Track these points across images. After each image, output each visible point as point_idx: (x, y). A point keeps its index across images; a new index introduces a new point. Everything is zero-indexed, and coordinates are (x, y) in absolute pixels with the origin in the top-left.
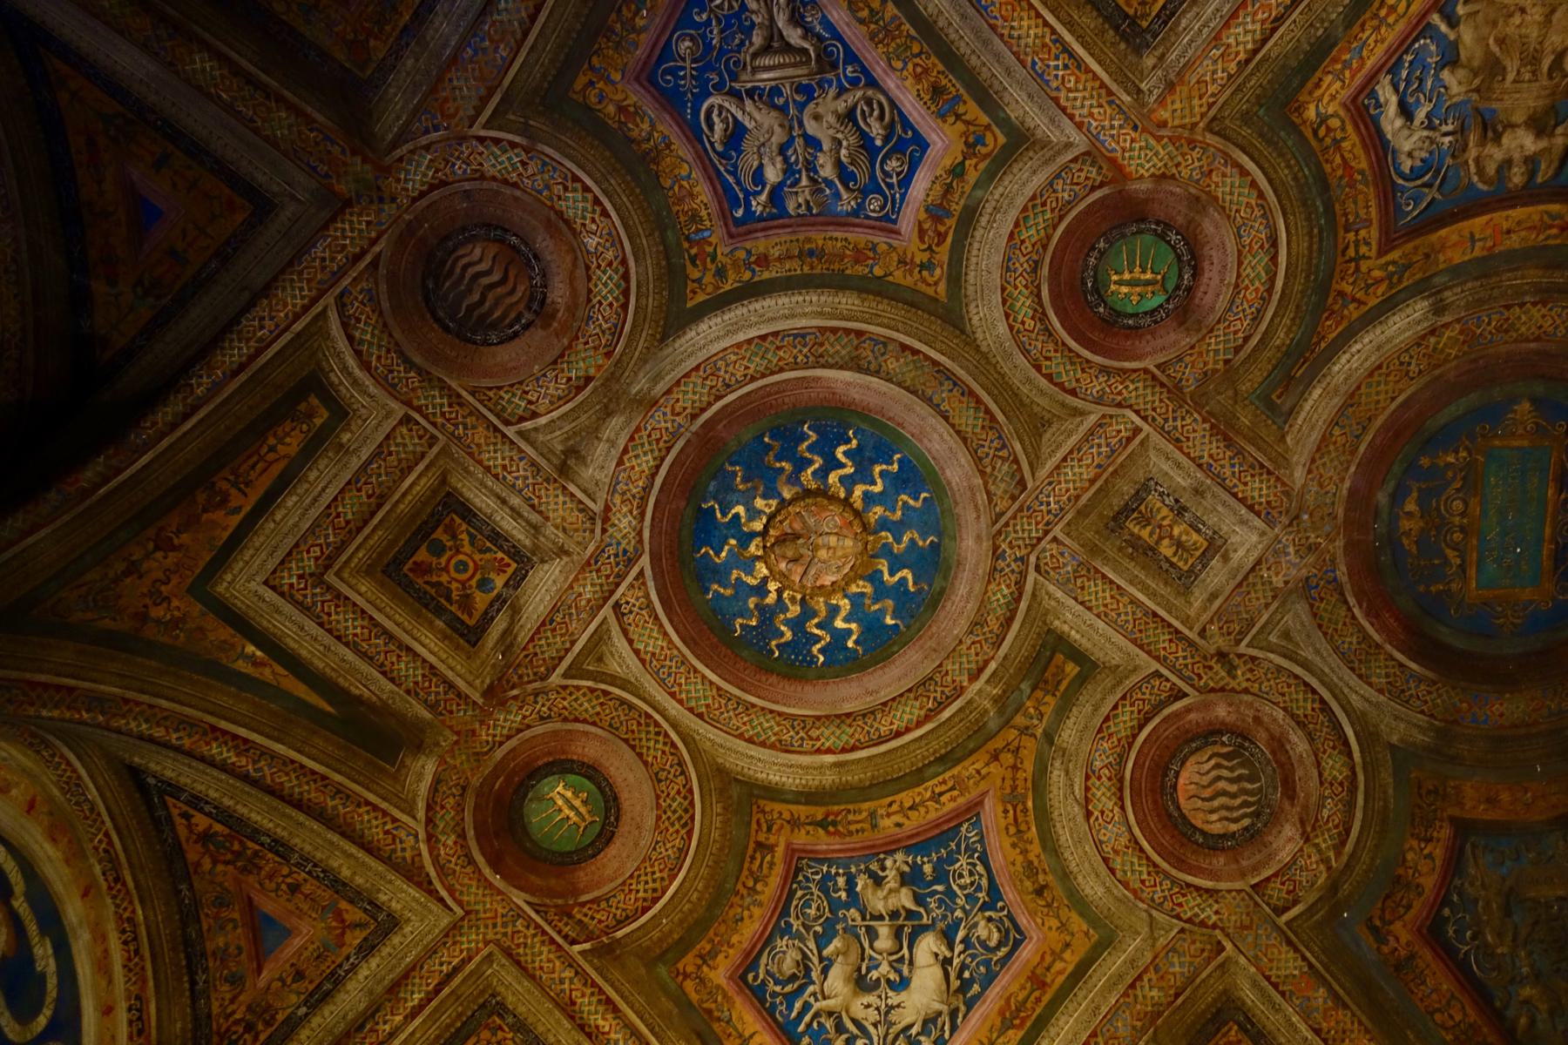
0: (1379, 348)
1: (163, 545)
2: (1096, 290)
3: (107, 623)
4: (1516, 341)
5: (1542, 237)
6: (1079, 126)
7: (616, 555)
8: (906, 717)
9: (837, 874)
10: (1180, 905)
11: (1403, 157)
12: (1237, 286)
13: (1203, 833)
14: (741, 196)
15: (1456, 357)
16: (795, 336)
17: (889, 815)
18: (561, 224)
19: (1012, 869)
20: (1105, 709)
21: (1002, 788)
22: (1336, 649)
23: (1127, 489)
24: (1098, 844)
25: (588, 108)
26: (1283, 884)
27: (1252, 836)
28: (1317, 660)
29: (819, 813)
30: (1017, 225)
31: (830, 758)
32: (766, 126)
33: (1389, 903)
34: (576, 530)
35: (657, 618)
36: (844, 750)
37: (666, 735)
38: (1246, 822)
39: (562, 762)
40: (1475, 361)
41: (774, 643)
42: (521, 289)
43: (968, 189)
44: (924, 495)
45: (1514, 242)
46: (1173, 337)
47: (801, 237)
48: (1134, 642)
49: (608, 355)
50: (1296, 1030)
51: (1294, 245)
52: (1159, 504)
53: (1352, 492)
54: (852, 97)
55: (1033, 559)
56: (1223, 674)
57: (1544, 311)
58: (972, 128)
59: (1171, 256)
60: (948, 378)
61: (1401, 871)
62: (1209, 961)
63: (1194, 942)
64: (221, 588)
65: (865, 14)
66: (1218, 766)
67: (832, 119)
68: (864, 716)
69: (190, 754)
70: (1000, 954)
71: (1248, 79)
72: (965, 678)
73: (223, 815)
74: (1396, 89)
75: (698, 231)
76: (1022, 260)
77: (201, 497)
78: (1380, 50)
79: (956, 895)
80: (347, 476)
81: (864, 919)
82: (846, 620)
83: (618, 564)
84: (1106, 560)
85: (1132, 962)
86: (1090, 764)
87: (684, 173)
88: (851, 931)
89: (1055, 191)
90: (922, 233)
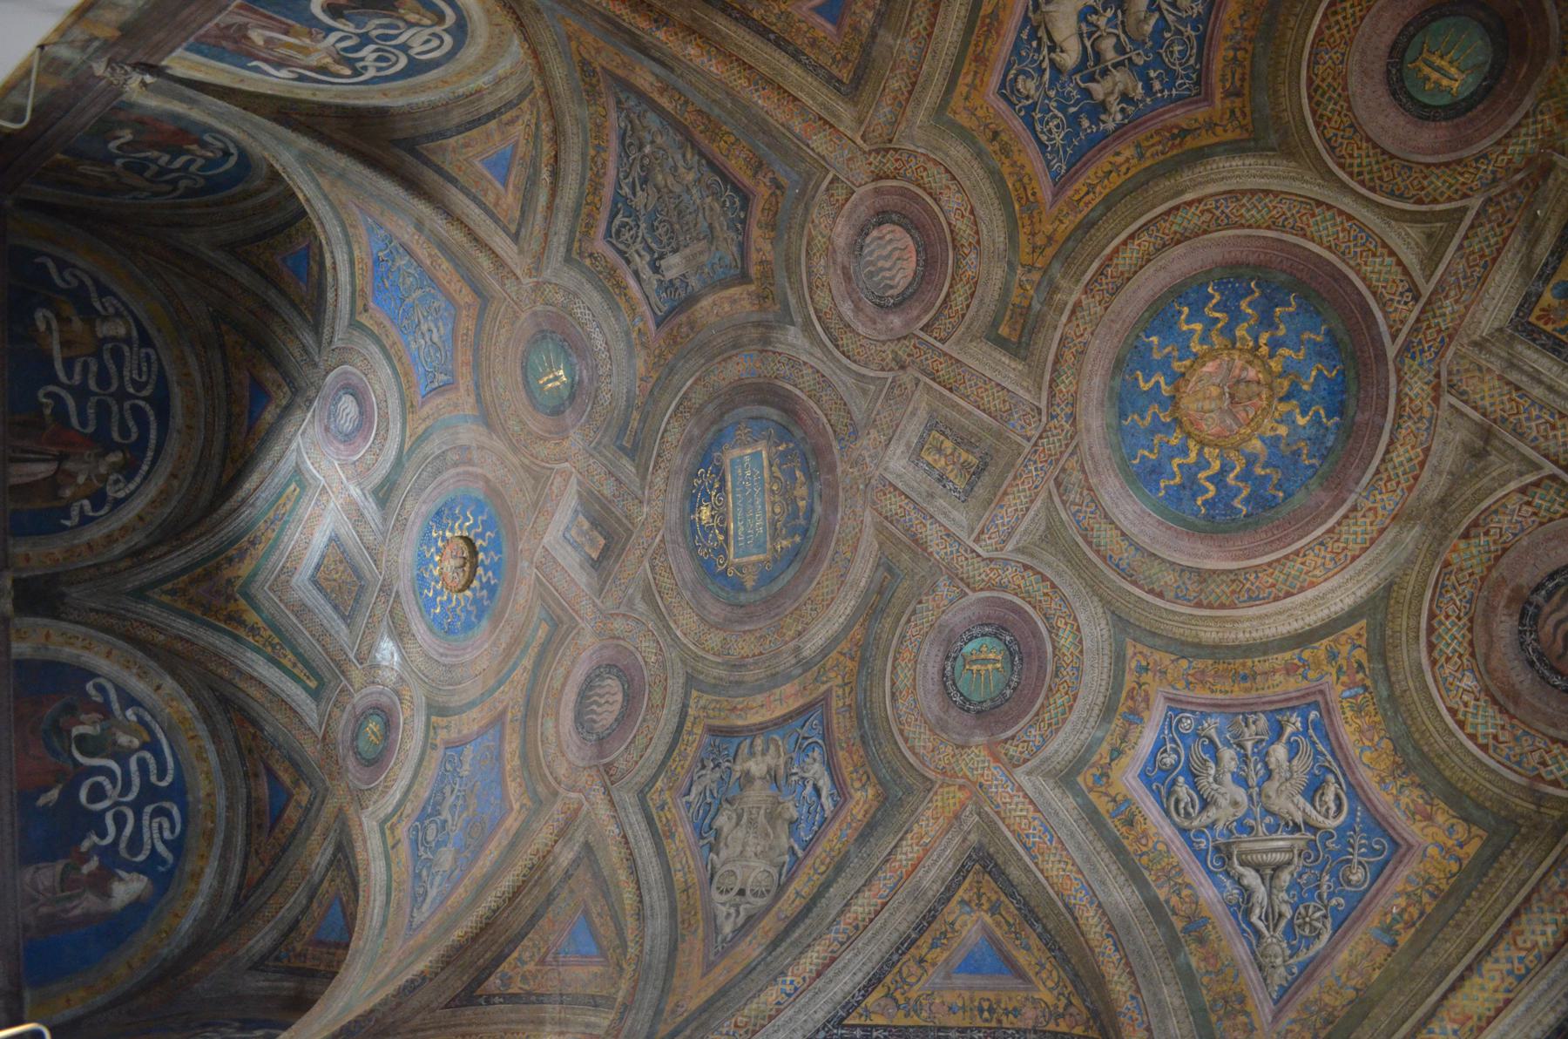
6: (1020, 788)
7: (1422, 351)
8: (1128, 254)
9: (1162, 91)
10: (897, 160)
12: (916, 662)
13: (893, 223)
14: (1311, 731)
16: (1257, 598)
17: (1127, 160)
18: (1501, 699)
19: (1020, 147)
20: (975, 302)
21: (1040, 213)
23: (981, 491)
24: (961, 189)
25: (1467, 819)
28: (845, 378)
29: (1190, 143)
30: (1071, 707)
31: (1188, 197)
32: (1283, 797)
34: (1467, 370)
35: (1374, 294)
36: (1177, 208)
37: (1351, 175)
38: (868, 240)
39: (1458, 115)
41: (1257, 294)
42: (1549, 627)
43: (1108, 738)
44: (1136, 462)
45: (760, 699)
47: (1254, 694)
49: (1447, 564)
52: (956, 481)
53: (836, 510)
54: (1204, 819)
55: (1044, 419)
56: (900, 353)
58: (1103, 789)
60: (1123, 570)
61: (772, 234)
65: (1185, 892)
66: (892, 278)
67: (1223, 802)
68: (1164, 245)
70: (1013, 72)
71: (907, 819)
72: (1084, 303)
75: (1355, 697)
76: (1067, 678)
78: (830, 835)
79: (1057, 108)
81: (1130, 59)
83: (1420, 343)
84: (989, 430)
85: (918, 103)
86: (979, 254)
87: (1368, 753)
88: (1138, 43)
90: (1147, 700)
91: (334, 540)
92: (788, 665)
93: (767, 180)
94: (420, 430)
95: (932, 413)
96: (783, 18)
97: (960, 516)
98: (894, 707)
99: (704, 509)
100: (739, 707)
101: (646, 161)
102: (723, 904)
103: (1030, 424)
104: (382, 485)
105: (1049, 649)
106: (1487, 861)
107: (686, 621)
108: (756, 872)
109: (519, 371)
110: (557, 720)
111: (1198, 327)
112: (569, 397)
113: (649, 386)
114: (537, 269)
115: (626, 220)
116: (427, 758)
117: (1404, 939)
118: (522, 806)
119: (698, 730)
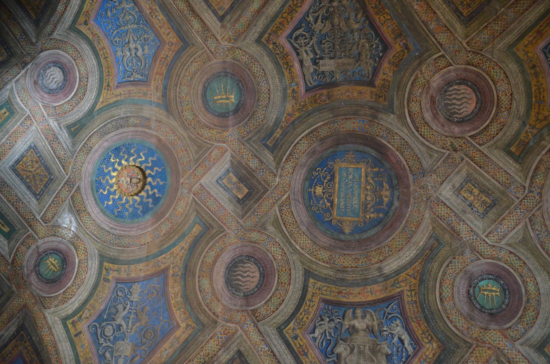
0: (399, 257)
2: (504, 290)
5: (348, 290)
6: (519, 352)
10: (480, 60)
11: (400, 325)
13: (467, 85)
15: (372, 251)
21: (544, 106)
22: (413, 150)
23: (491, 215)
24: (509, 83)
26: (439, 66)
27: (449, 83)
28: (419, 146)
30: (537, 318)
33: (401, 58)
38: (451, 89)
45: (357, 290)
46: (475, 269)
48: (488, 158)
50: (441, 13)
51: (434, 298)
52: (479, 208)
53: (408, 206)
55: (526, 192)
56: (455, 143)
57: (344, 264)
59: (478, 299)
61: (395, 69)
62: (472, 39)
63: (478, 46)
66: (459, 110)
74: (406, 349)
76: (533, 304)
84: (498, 189)
85: (502, 39)
86: (509, 114)
89: (524, 328)
91: (33, 148)
93: (401, 44)
94: (112, 101)
99: (318, 188)
100: (344, 292)
103: (519, 192)
104: (74, 124)
109: (200, 88)
110: (211, 280)
112: (234, 110)
113: (293, 119)
114: (235, 40)
116: (100, 285)
118: (187, 326)
119: (316, 300)
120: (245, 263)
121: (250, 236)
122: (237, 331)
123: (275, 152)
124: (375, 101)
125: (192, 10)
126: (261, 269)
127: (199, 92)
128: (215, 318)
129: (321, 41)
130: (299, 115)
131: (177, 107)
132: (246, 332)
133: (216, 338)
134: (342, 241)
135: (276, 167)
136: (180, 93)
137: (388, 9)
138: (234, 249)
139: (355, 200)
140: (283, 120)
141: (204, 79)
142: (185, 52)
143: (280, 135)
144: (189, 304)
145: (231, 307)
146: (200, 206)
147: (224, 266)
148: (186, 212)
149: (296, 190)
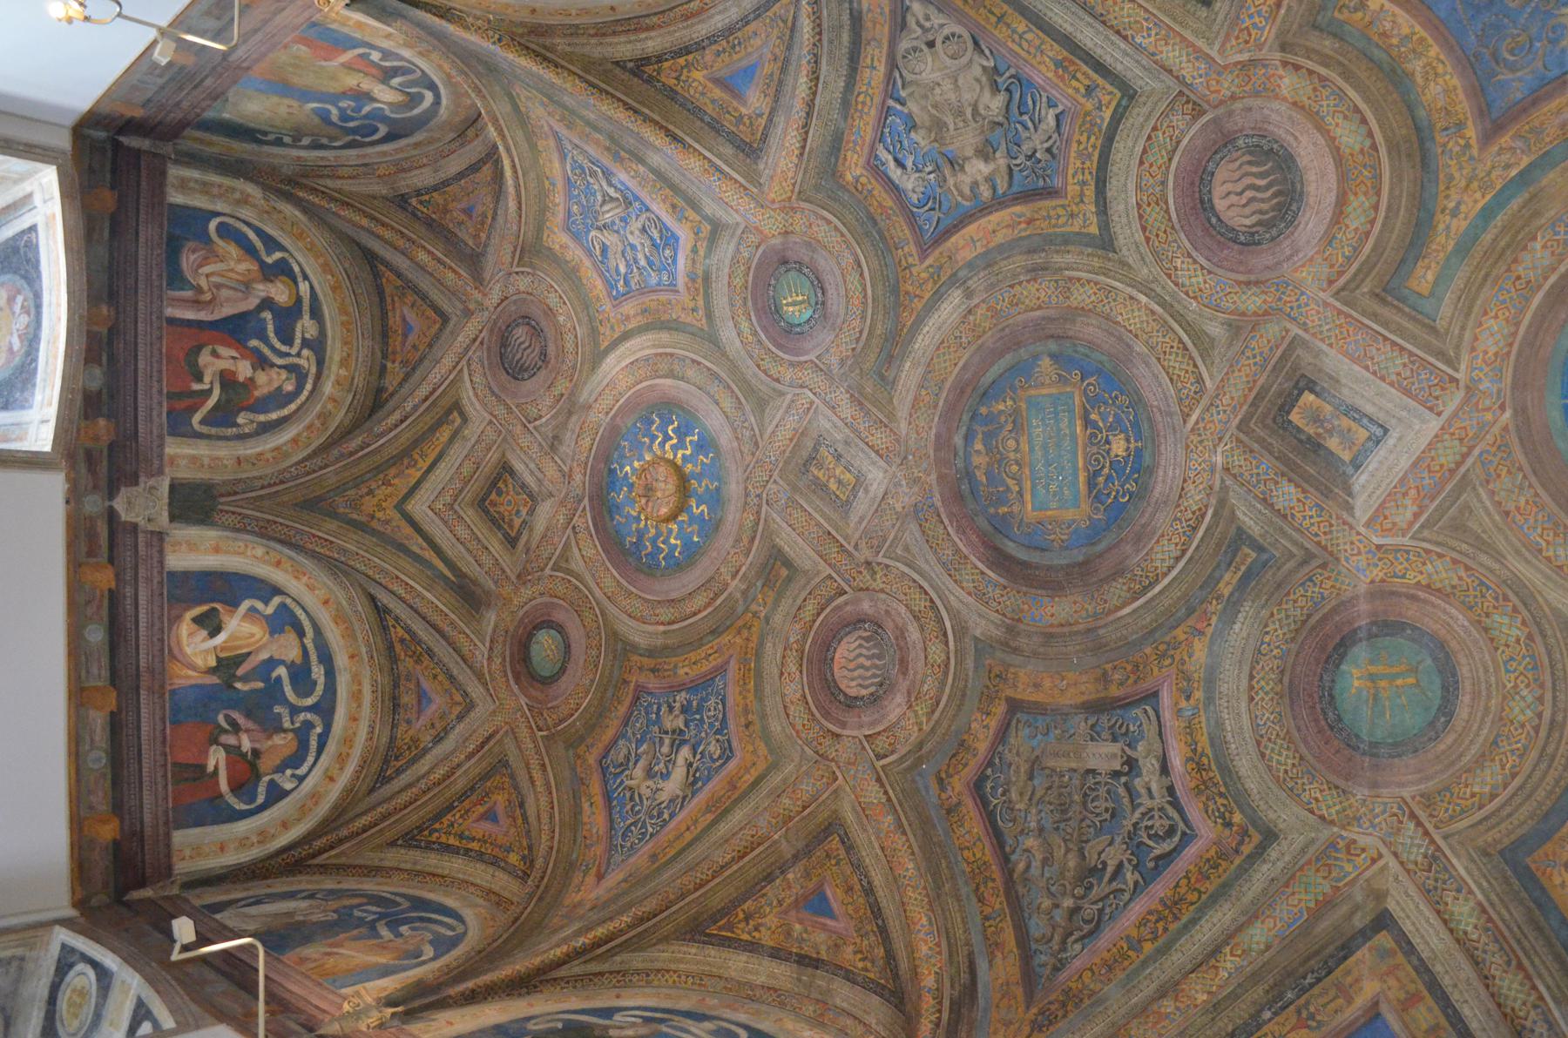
0: (939, 329)
1: (387, 483)
3: (355, 516)
4: (1026, 311)
6: (736, 211)
11: (910, 194)
13: (845, 695)
20: (799, 602)
22: (939, 560)
31: (662, 628)
33: (953, 760)
36: (669, 624)
38: (872, 689)
40: (1003, 329)
45: (1000, 238)
48: (818, 553)
50: (873, 848)
53: (938, 436)
57: (1036, 286)
61: (966, 737)
64: (409, 507)
66: (860, 646)
67: (637, 232)
69: (386, 588)
73: (408, 630)
77: (406, 461)
78: (869, 129)
80: (465, 452)
82: (676, 539)
86: (787, 639)
90: (688, 289)
92: (975, 279)
95: (845, 516)
96: (862, 932)
97: (824, 424)
98: (856, 255)
99: (1121, 452)
100: (1023, 226)
101: (1079, 891)
102: (942, 26)
105: (753, 318)
106: (540, 229)
107: (1135, 314)
108: (928, 69)
109: (1462, 712)
111: (672, 541)
112: (1354, 643)
113: (1190, 622)
115: (1151, 843)
117: (547, 183)
119: (1073, 189)
120: (1259, 223)
121: (1264, 297)
122: (1222, 51)
123: (1233, 531)
124: (1010, 665)
125: (1477, 964)
126: (1214, 220)
127: (1467, 699)
128: (1290, 58)
129: (1113, 816)
130: (1175, 633)
131: (1549, 654)
132: (1199, 54)
133: (1265, 8)
134: (1052, 337)
135: (1227, 492)
136: (1540, 699)
137: (964, 872)
138: (1297, 252)
139: (1038, 436)
140: (1214, 619)
141: (1450, 739)
142: (1520, 832)
143: (1221, 577)
144: (1380, 68)
145: (1259, 102)
146: (1427, 348)
147: (1312, 200)
148: (1470, 324)
149: (1171, 439)
